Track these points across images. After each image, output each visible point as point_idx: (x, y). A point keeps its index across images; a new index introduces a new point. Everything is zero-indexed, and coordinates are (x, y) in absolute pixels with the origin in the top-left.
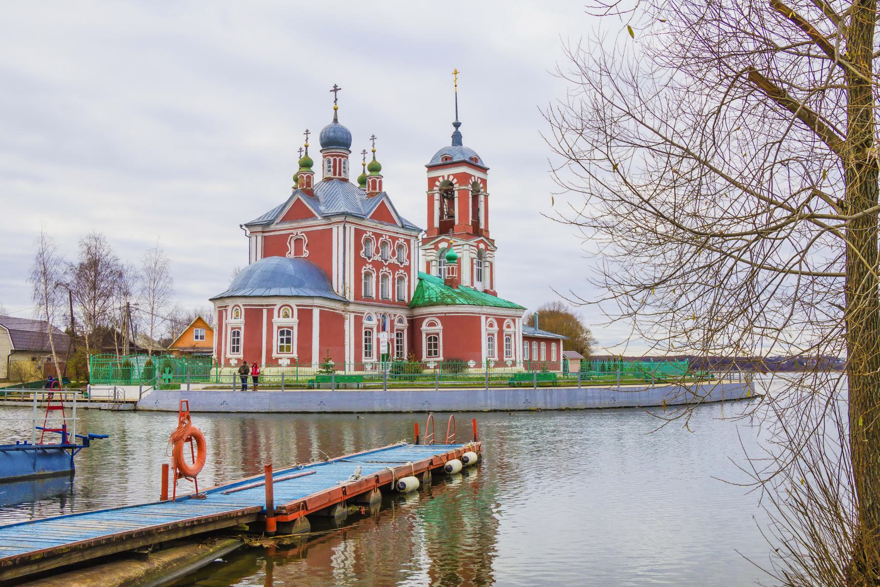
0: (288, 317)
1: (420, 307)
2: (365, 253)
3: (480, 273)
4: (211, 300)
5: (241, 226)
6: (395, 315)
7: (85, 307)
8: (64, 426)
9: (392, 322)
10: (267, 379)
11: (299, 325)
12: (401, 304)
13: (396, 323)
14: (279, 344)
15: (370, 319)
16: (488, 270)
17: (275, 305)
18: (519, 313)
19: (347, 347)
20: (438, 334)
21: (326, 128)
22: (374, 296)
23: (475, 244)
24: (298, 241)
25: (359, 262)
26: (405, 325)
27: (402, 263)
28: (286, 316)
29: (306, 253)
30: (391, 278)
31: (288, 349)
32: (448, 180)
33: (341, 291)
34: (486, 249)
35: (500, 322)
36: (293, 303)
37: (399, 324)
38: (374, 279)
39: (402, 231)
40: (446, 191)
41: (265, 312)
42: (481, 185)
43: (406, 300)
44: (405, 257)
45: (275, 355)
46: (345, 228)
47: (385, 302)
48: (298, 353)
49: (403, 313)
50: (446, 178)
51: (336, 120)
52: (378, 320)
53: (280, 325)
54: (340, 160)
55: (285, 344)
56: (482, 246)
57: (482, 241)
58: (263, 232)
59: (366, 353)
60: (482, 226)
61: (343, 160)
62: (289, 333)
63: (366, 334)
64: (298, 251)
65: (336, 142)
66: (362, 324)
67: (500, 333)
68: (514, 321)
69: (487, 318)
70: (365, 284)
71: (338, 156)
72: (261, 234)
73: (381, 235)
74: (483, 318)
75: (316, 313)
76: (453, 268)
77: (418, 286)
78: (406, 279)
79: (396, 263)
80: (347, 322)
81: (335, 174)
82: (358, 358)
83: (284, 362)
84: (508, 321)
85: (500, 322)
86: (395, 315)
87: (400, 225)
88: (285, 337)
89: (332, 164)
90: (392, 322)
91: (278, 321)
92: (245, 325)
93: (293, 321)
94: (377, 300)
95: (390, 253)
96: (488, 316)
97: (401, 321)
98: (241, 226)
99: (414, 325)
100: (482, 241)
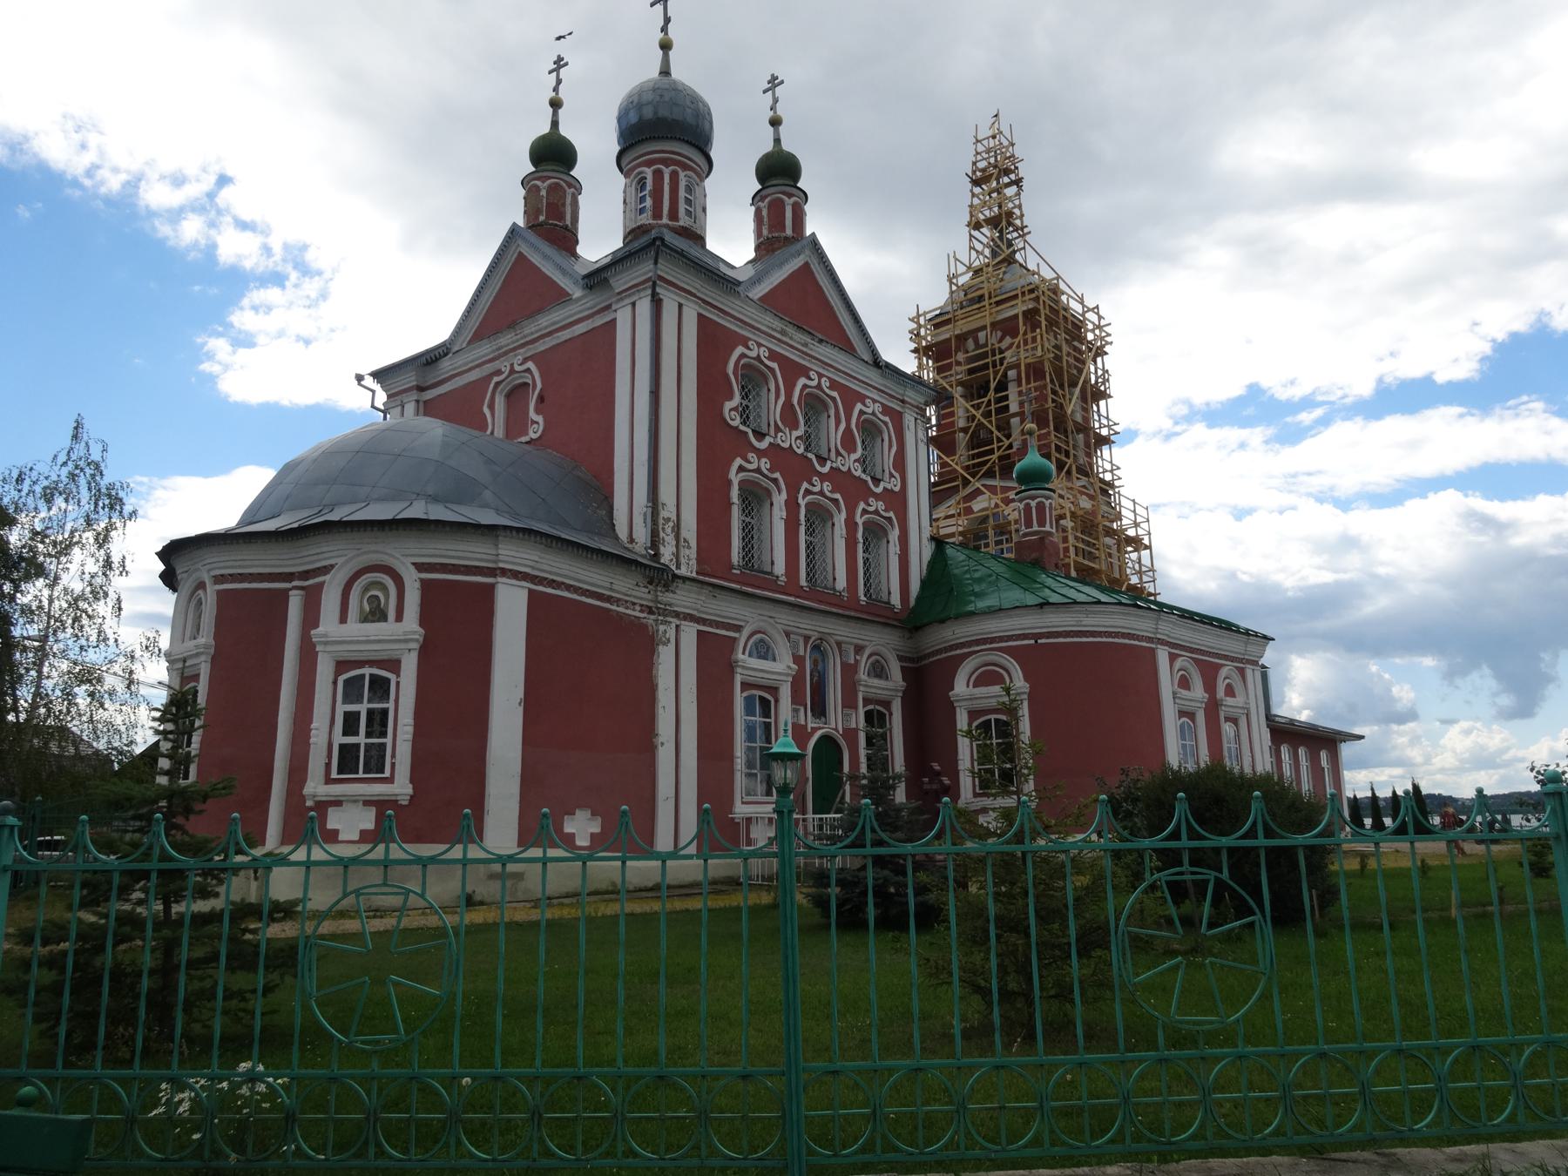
0: (383, 617)
5: (359, 378)
6: (859, 649)
9: (849, 671)
10: (1268, 768)
11: (425, 652)
12: (875, 613)
13: (862, 675)
14: (339, 739)
17: (326, 570)
19: (665, 756)
21: (630, 96)
22: (780, 568)
24: (517, 394)
25: (717, 443)
27: (877, 481)
28: (376, 614)
29: (537, 425)
31: (376, 760)
33: (642, 534)
35: (1209, 673)
36: (404, 555)
38: (779, 513)
43: (896, 600)
44: (889, 461)
45: (315, 787)
46: (657, 303)
47: (816, 598)
49: (882, 642)
51: (665, 71)
52: (798, 660)
53: (346, 652)
54: (674, 175)
58: (421, 389)
62: (380, 687)
64: (516, 424)
65: (665, 132)
66: (731, 667)
67: (1213, 707)
68: (1242, 671)
69: (1173, 658)
71: (666, 162)
72: (414, 396)
74: (1163, 656)
76: (1041, 507)
77: (931, 564)
78: (894, 534)
80: (665, 655)
81: (657, 214)
83: (351, 823)
85: (1209, 673)
88: (362, 708)
89: (649, 186)
90: (849, 671)
91: (339, 632)
92: (214, 660)
93: (402, 632)
94: (792, 585)
95: (836, 437)
97: (879, 671)
98: (359, 378)
99: (926, 686)
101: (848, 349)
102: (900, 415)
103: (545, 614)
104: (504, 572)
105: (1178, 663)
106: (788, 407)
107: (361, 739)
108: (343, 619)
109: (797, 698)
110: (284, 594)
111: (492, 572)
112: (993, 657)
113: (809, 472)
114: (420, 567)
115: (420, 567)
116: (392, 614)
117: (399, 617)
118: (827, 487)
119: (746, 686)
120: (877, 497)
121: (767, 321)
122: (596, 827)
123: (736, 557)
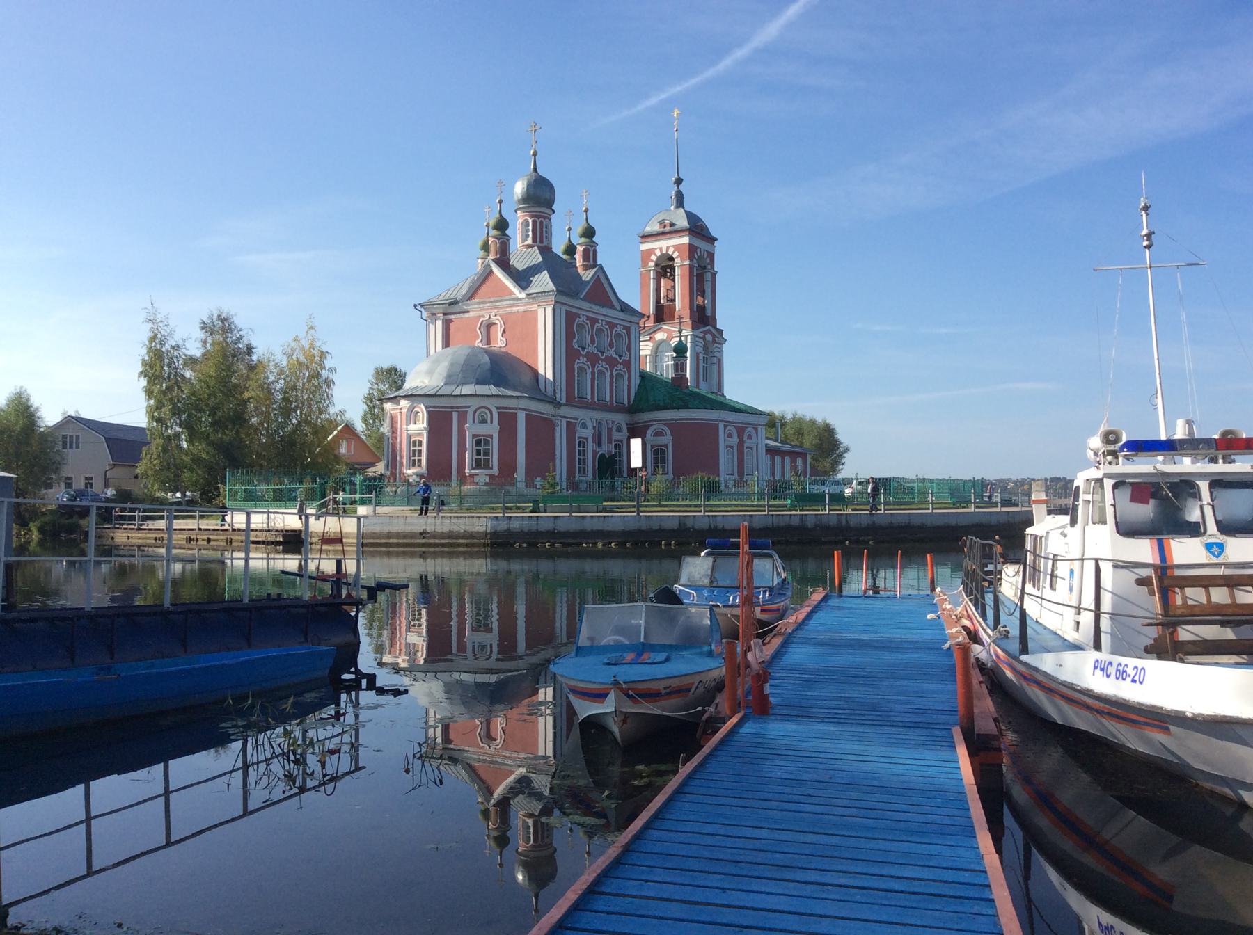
1: (642, 411)
3: (705, 369)
7: (1034, 561)
8: (364, 767)
12: (619, 408)
15: (584, 426)
16: (715, 367)
20: (666, 446)
28: (484, 421)
30: (608, 375)
31: (487, 465)
34: (714, 342)
35: (741, 430)
39: (621, 315)
40: (664, 268)
41: (455, 415)
43: (626, 402)
51: (535, 169)
56: (709, 337)
60: (709, 313)
62: (487, 443)
65: (540, 196)
68: (756, 430)
69: (725, 427)
71: (539, 217)
74: (721, 426)
75: (521, 417)
80: (558, 429)
82: (570, 473)
84: (750, 430)
85: (741, 430)
90: (610, 430)
91: (471, 429)
93: (493, 429)
95: (607, 344)
97: (619, 430)
100: (708, 332)
101: (612, 307)
103: (530, 419)
107: (482, 457)
109: (594, 441)
121: (586, 305)
122: (538, 479)
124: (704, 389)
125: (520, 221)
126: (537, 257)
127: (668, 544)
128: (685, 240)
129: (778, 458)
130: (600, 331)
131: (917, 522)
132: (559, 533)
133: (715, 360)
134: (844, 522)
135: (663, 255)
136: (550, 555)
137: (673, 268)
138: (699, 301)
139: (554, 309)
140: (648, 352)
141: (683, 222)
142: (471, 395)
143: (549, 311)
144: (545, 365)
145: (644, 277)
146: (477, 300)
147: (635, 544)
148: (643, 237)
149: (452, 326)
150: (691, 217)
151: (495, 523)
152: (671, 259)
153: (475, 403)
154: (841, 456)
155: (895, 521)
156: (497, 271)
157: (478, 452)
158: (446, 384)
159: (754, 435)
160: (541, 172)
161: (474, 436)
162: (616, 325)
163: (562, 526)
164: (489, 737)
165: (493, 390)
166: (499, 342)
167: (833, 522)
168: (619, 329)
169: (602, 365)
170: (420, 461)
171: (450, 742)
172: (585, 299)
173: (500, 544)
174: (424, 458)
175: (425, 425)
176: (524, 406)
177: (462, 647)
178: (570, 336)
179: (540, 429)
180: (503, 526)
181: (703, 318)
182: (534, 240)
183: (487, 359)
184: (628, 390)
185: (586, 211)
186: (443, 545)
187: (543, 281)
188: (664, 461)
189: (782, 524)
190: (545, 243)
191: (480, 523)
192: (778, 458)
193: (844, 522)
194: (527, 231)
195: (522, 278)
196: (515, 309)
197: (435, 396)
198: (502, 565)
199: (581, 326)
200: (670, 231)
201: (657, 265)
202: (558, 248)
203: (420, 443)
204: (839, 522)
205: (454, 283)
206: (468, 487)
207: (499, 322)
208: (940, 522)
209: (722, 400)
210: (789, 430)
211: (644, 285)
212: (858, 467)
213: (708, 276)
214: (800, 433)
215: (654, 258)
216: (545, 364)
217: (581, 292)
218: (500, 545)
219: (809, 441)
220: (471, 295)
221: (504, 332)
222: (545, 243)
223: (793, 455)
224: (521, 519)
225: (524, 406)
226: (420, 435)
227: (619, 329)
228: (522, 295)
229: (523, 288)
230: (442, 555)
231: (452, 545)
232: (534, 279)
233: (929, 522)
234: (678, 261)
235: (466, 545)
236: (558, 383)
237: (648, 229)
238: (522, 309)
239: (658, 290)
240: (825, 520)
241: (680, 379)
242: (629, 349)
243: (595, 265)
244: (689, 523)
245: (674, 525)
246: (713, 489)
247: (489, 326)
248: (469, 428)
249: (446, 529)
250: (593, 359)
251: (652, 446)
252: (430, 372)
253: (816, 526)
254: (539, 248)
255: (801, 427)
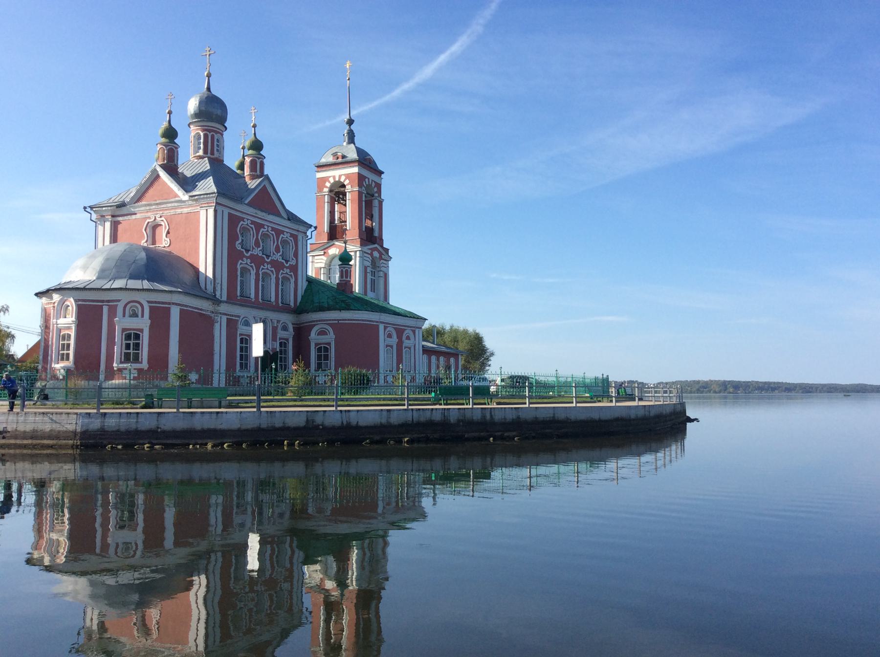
0: (137, 316)
2: (242, 243)
3: (373, 282)
4: (37, 294)
5: (85, 208)
12: (285, 309)
14: (124, 351)
17: (119, 301)
18: (419, 323)
20: (329, 344)
23: (369, 252)
26: (289, 334)
27: (287, 261)
28: (134, 315)
31: (136, 359)
32: (339, 181)
34: (381, 258)
35: (400, 332)
37: (283, 332)
38: (253, 277)
40: (338, 194)
42: (376, 190)
43: (292, 304)
44: (292, 255)
48: (149, 362)
49: (287, 319)
50: (337, 179)
51: (209, 89)
54: (213, 137)
55: (131, 351)
56: (376, 254)
57: (376, 249)
59: (241, 364)
60: (376, 234)
61: (216, 137)
62: (137, 337)
63: (242, 342)
65: (213, 113)
68: (414, 332)
69: (385, 328)
70: (242, 282)
71: (210, 131)
73: (262, 226)
74: (381, 327)
75: (175, 313)
79: (281, 260)
82: (230, 366)
84: (408, 332)
85: (400, 332)
86: (278, 321)
87: (285, 216)
93: (143, 323)
95: (273, 248)
96: (386, 325)
97: (285, 328)
98: (85, 208)
100: (376, 249)
101: (278, 215)
102: (297, 236)
103: (185, 314)
104: (173, 304)
105: (388, 329)
106: (257, 241)
107: (131, 351)
108: (124, 316)
110: (101, 307)
111: (169, 304)
112: (325, 326)
113: (263, 262)
114: (149, 302)
115: (149, 302)
116: (140, 315)
117: (143, 316)
118: (269, 266)
119: (241, 335)
120: (287, 268)
121: (251, 210)
123: (239, 294)
124: (370, 296)
125: (193, 134)
126: (206, 165)
127: (291, 445)
128: (355, 170)
129: (433, 358)
130: (265, 236)
131: (561, 416)
132: (164, 432)
133: (381, 274)
134: (488, 417)
135: (335, 182)
136: (152, 459)
137: (344, 194)
138: (368, 223)
139: (215, 211)
140: (323, 265)
141: (353, 155)
142: (121, 289)
143: (211, 212)
144: (205, 263)
145: (319, 200)
146: (143, 203)
147: (254, 444)
148: (318, 167)
149: (120, 227)
150: (359, 151)
151: (86, 421)
152: (344, 186)
153: (125, 297)
154: (488, 359)
155: (541, 416)
156: (163, 175)
157: (128, 346)
158: (98, 278)
159: (412, 336)
160: (214, 92)
161: (124, 330)
162: (283, 232)
163: (167, 425)
164: (145, 630)
165: (146, 284)
166: (163, 243)
167: (477, 416)
168: (286, 236)
169: (267, 268)
170: (68, 355)
171: (106, 631)
172: (250, 204)
173: (92, 445)
174: (71, 352)
175: (74, 319)
176: (178, 303)
177: (105, 546)
178: (232, 238)
179: (197, 327)
180: (96, 424)
181: (371, 237)
182: (205, 152)
183: (143, 255)
184: (294, 294)
185: (254, 126)
186: (25, 447)
187: (209, 185)
188: (326, 358)
189: (422, 419)
190: (216, 155)
191: (69, 419)
192: (433, 358)
193: (488, 417)
194: (199, 143)
195: (187, 184)
196: (179, 211)
197: (84, 289)
198: (94, 469)
199: (245, 230)
200: (344, 162)
201: (331, 191)
202: (231, 161)
203: (69, 336)
204: (484, 417)
205: (124, 187)
206: (116, 382)
207: (164, 224)
208: (582, 417)
209: (388, 306)
210: (447, 338)
211: (320, 208)
212: (497, 371)
213: (376, 203)
214: (455, 340)
215: (328, 185)
216: (205, 261)
217: (248, 203)
218: (94, 446)
219: (462, 346)
220: (139, 197)
221: (168, 233)
222: (216, 155)
223: (447, 355)
224: (116, 417)
225: (178, 303)
226: (69, 328)
227: (286, 236)
228: (184, 197)
229: (187, 191)
230: (23, 458)
231: (34, 447)
232: (199, 184)
233: (573, 417)
234: (348, 188)
235: (51, 447)
236: (218, 281)
237: (324, 160)
238: (185, 210)
239: (332, 213)
240: (468, 415)
241: (345, 285)
242: (296, 255)
243: (262, 174)
244: (319, 420)
245: (301, 422)
246: (361, 384)
247: (155, 227)
248: (119, 321)
249: (29, 428)
250: (258, 261)
251: (316, 345)
252: (85, 268)
253: (459, 421)
254: (209, 158)
255: (456, 335)
